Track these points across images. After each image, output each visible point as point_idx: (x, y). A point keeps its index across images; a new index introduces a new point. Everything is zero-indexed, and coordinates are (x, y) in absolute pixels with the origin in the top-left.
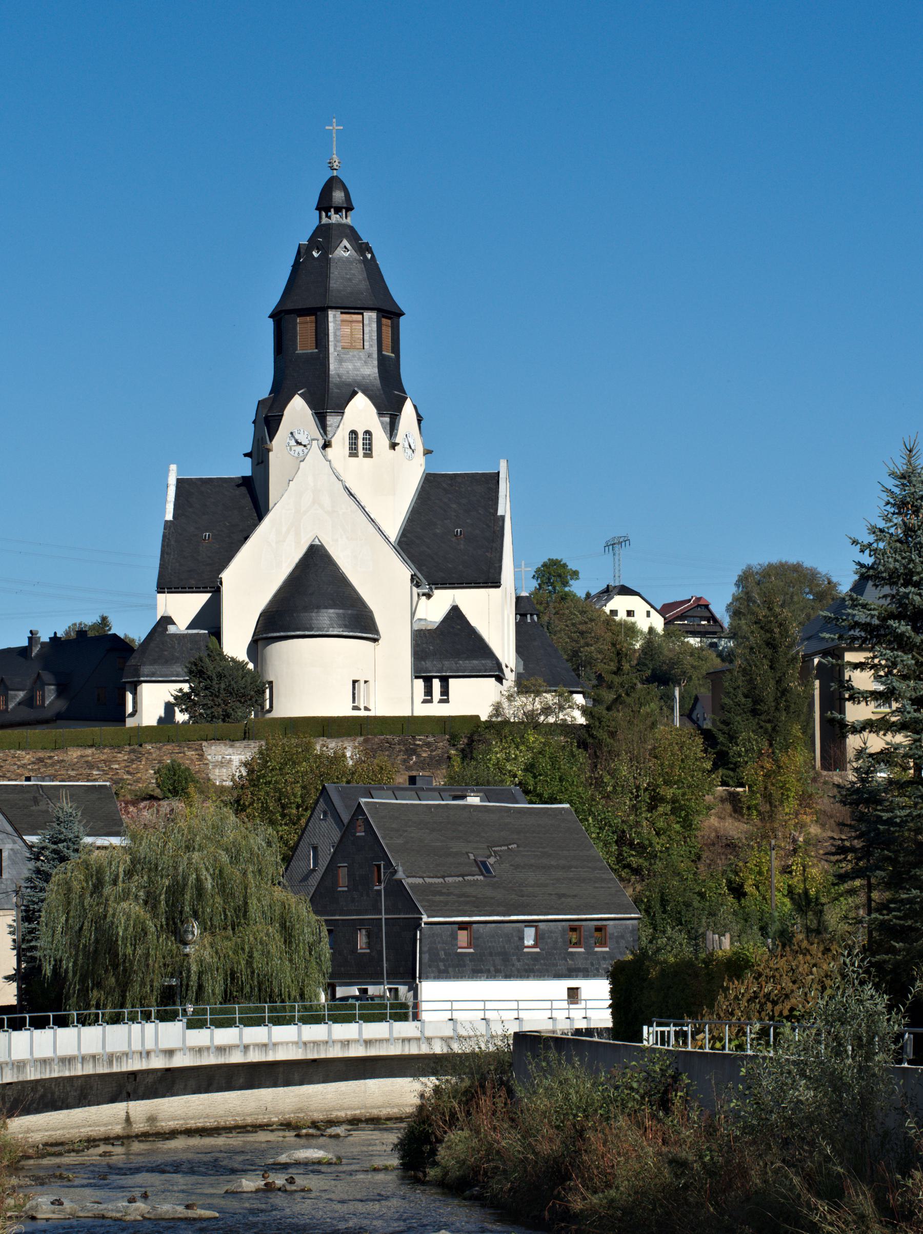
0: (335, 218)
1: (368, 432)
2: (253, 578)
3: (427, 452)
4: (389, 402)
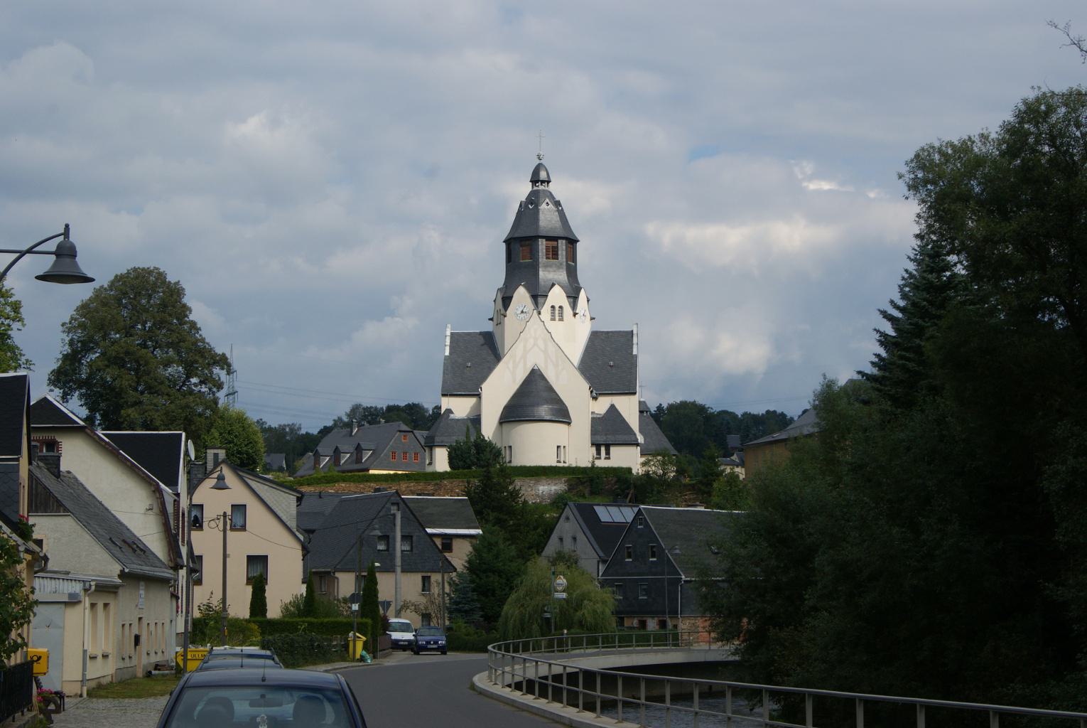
2: (499, 387)
3: (592, 319)
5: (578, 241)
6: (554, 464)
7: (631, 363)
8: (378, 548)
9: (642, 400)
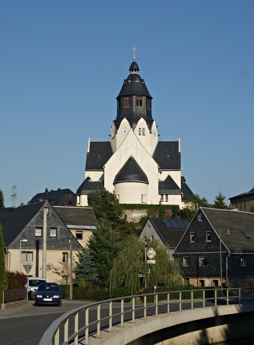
0: (134, 72)
1: (140, 135)
2: (114, 166)
3: (159, 135)
4: (150, 122)
5: (152, 98)
6: (140, 203)
7: (178, 156)
8: (36, 235)
9: (182, 176)
